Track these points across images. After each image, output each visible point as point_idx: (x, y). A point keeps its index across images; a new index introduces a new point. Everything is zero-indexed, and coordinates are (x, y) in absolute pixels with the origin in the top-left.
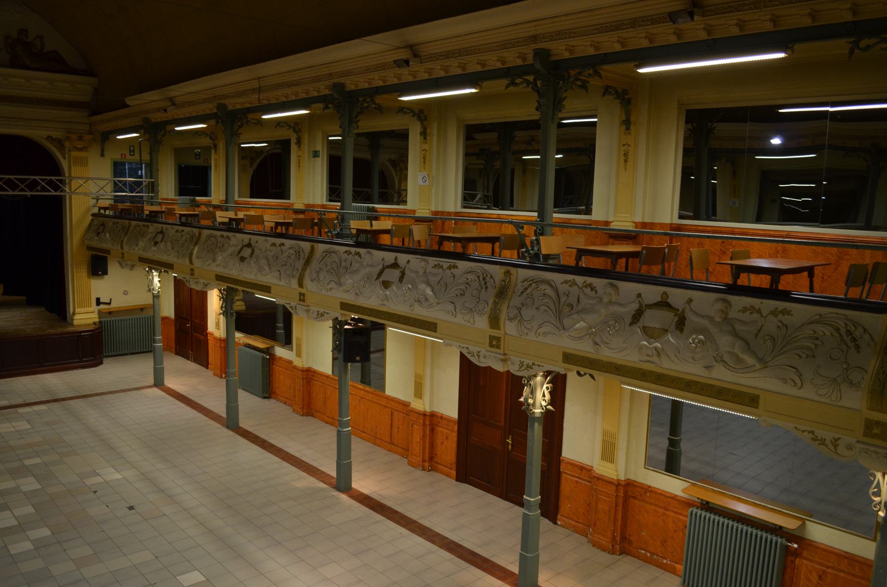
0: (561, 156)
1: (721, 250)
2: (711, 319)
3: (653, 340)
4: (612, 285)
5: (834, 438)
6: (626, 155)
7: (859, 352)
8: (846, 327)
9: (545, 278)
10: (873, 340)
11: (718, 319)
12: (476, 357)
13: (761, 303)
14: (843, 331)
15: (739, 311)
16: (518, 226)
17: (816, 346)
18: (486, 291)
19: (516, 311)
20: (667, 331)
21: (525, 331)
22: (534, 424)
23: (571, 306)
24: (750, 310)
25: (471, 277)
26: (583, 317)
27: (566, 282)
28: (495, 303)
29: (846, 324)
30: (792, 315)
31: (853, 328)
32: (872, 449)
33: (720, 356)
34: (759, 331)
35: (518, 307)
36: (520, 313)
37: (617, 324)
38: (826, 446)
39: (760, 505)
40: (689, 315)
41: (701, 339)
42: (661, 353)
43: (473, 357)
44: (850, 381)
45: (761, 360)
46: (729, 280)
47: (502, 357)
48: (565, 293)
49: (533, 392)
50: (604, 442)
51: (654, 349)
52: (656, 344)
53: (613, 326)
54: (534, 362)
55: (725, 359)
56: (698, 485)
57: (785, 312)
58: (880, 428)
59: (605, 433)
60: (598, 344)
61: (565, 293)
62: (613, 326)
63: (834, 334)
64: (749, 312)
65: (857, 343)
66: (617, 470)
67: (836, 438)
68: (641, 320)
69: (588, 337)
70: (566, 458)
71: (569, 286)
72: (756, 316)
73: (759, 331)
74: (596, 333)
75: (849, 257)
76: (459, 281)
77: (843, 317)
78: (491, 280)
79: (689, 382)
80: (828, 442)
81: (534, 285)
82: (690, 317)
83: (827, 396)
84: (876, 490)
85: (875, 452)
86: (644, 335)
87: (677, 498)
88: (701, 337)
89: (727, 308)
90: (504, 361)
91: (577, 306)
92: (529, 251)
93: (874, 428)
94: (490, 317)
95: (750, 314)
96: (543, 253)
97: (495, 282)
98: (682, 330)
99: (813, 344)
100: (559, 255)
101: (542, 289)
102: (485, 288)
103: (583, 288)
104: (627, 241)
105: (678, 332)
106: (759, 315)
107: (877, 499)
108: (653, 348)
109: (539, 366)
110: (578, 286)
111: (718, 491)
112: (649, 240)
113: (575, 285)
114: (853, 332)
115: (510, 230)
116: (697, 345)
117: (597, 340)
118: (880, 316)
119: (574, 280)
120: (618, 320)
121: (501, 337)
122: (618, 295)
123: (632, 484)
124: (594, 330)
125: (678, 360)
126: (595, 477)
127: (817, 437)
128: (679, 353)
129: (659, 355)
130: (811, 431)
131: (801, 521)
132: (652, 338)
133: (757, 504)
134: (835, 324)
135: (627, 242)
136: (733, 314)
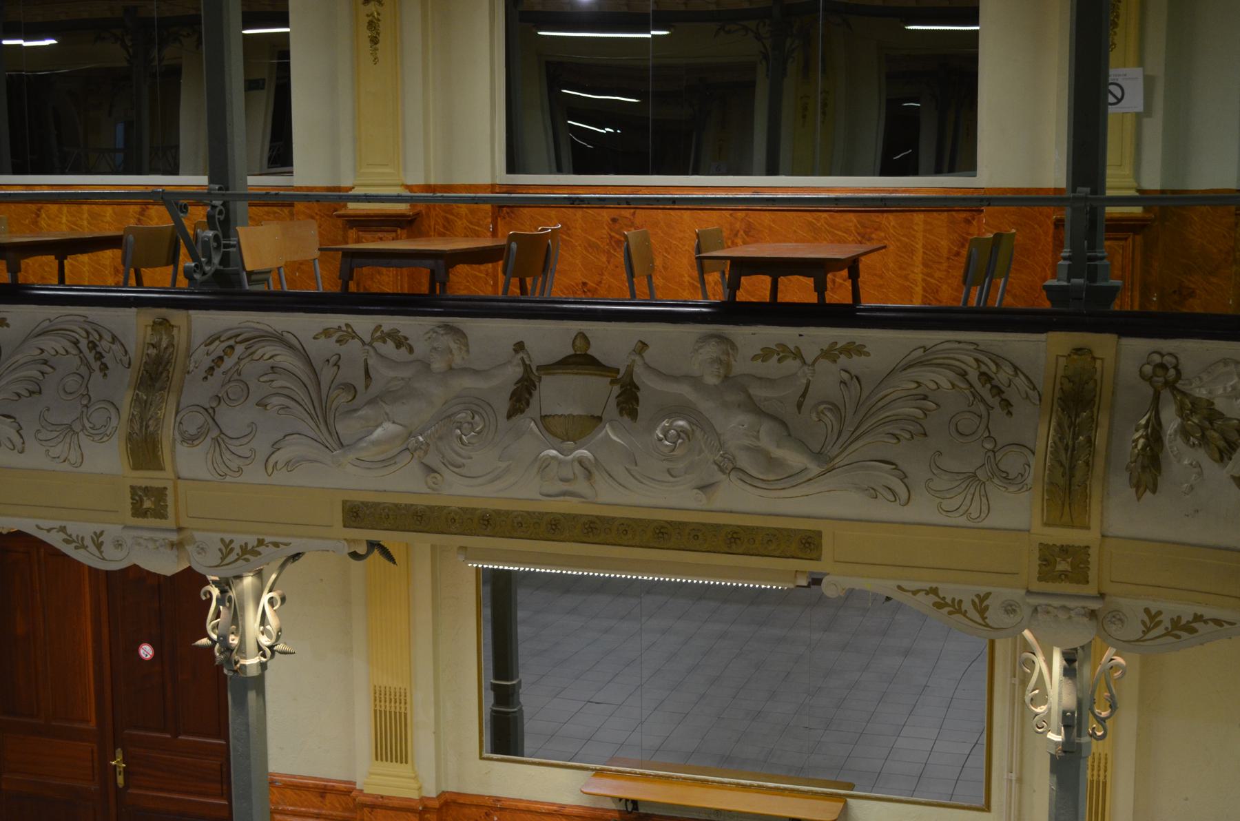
0: (53, 42)
1: (611, 237)
2: (695, 381)
3: (570, 444)
4: (447, 327)
5: (978, 596)
6: (372, 25)
7: (1010, 413)
8: (979, 367)
9: (269, 329)
10: (1034, 388)
11: (711, 380)
12: (92, 548)
13: (801, 335)
14: (973, 375)
15: (755, 358)
16: (176, 204)
17: (925, 412)
18: (105, 375)
19: (200, 419)
20: (600, 419)
21: (235, 463)
22: (246, 695)
23: (351, 388)
24: (778, 354)
25: (51, 344)
26: (388, 411)
27: (327, 333)
28: (142, 406)
29: (977, 360)
30: (867, 354)
31: (994, 368)
32: (1056, 602)
33: (729, 459)
34: (804, 395)
35: (207, 406)
36: (213, 419)
37: (477, 417)
38: (965, 614)
39: (751, 786)
40: (643, 378)
41: (681, 426)
42: (593, 470)
43: (82, 551)
44: (1004, 475)
45: (818, 456)
46: (717, 294)
47: (174, 537)
48: (328, 361)
49: (237, 618)
50: (379, 716)
51: (576, 464)
52: (579, 451)
53: (469, 423)
54: (261, 537)
55: (740, 464)
56: (611, 771)
57: (852, 349)
58: (1069, 560)
59: (379, 695)
60: (435, 471)
61: (328, 361)
62: (469, 423)
63: (956, 383)
64: (776, 357)
65: (1004, 396)
66: (416, 778)
67: (982, 595)
68: (534, 402)
69: (407, 457)
70: (280, 775)
71: (337, 341)
72: (792, 364)
73: (804, 395)
74: (428, 445)
75: (882, 234)
76: (18, 357)
77: (972, 347)
78: (114, 347)
79: (662, 527)
80: (967, 605)
81: (239, 349)
82: (648, 383)
83: (961, 511)
84: (1037, 692)
85: (1064, 608)
86: (547, 434)
87: (567, 811)
88: (681, 423)
89: (728, 354)
90: (178, 546)
91: (367, 387)
92: (202, 266)
93: (1058, 559)
94: (130, 438)
95: (780, 360)
96: (249, 268)
97: (126, 352)
98: (633, 415)
99: (917, 408)
100: (269, 272)
101: (266, 357)
102: (101, 370)
103: (375, 344)
104: (396, 231)
105: (626, 418)
106: (798, 363)
107: (1041, 709)
108: (573, 461)
109: (276, 545)
110: (361, 339)
111: (655, 776)
112: (444, 227)
113: (353, 338)
114: (993, 376)
115: (159, 218)
116: (675, 443)
117: (433, 460)
118: (1043, 337)
119: (347, 325)
120: (475, 408)
121: (165, 488)
122: (468, 351)
123: (455, 802)
124: (421, 438)
125: (636, 482)
126: (364, 805)
127: (944, 598)
128: (636, 465)
129: (589, 475)
130: (931, 588)
131: (841, 802)
132: (568, 440)
133: (744, 786)
134: (957, 363)
135: (394, 235)
136: (740, 366)
